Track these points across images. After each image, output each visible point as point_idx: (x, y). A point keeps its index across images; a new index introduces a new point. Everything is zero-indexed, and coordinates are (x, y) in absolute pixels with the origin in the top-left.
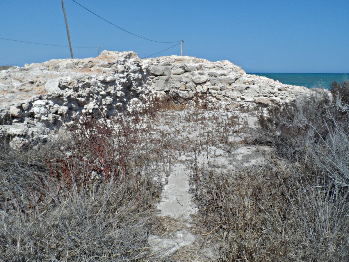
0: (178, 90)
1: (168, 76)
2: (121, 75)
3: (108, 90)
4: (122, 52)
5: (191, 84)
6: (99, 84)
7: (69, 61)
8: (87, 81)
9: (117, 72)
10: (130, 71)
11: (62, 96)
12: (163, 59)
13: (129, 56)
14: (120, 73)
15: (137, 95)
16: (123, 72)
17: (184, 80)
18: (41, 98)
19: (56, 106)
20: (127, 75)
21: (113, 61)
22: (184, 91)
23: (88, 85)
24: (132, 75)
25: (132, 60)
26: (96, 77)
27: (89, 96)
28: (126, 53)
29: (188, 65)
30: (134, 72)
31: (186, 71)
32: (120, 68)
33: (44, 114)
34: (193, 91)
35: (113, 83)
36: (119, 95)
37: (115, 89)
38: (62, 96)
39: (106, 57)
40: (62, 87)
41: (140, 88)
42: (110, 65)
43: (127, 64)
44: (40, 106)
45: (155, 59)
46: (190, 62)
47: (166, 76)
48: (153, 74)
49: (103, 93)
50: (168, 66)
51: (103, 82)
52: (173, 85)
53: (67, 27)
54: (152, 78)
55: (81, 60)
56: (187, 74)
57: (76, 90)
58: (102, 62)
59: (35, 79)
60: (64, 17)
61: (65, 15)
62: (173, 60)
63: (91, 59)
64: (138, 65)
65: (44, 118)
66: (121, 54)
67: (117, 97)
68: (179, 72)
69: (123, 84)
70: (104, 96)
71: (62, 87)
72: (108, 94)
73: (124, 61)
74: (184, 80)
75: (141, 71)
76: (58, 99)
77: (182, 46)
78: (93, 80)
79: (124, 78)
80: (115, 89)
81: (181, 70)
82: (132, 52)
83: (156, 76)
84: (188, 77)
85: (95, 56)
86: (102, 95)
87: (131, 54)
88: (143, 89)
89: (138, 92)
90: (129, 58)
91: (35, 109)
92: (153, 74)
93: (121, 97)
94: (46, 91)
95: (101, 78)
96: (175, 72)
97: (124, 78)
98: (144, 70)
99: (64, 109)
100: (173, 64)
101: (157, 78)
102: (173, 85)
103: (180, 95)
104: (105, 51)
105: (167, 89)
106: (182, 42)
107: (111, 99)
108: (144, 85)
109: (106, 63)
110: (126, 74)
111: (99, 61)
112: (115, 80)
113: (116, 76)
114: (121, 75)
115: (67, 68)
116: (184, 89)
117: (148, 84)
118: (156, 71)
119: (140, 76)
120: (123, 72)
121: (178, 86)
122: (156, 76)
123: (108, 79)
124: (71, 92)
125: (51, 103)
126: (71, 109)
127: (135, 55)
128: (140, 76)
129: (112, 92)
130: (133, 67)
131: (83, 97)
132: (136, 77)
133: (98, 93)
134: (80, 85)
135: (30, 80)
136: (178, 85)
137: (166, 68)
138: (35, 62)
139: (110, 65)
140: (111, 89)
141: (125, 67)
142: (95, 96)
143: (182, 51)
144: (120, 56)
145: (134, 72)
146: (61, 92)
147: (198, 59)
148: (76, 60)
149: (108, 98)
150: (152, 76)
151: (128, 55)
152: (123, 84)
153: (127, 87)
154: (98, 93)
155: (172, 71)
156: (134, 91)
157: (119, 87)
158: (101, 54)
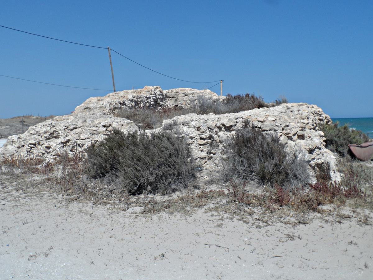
0: (182, 105)
1: (176, 98)
2: (153, 96)
3: (148, 101)
4: (154, 86)
5: (188, 102)
6: (144, 98)
7: (132, 90)
8: (140, 96)
9: (151, 94)
10: (157, 94)
11: (133, 100)
12: (175, 90)
13: (157, 88)
14: (153, 95)
15: (160, 106)
16: (154, 94)
17: (185, 99)
18: (127, 100)
19: (131, 103)
20: (156, 96)
21: (149, 90)
22: (185, 105)
23: (141, 98)
24: (158, 96)
25: (158, 90)
26: (143, 95)
27: (141, 102)
28: (155, 87)
29: (187, 92)
30: (159, 95)
31: (186, 95)
32: (153, 93)
33: (129, 104)
34: (189, 105)
35: (149, 98)
36: (152, 103)
37: (150, 100)
38: (133, 100)
39: (147, 88)
40: (133, 97)
41: (162, 103)
42: (149, 91)
43: (155, 91)
44: (127, 102)
45: (170, 90)
46: (188, 90)
47: (175, 98)
48: (169, 97)
49: (146, 101)
50: (177, 93)
51: (146, 97)
52: (180, 102)
53: (112, 74)
54: (168, 99)
55: (137, 90)
56: (186, 97)
57: (137, 98)
58: (145, 90)
59: (122, 96)
60: (110, 66)
61: (111, 64)
62: (180, 90)
63: (141, 89)
64: (161, 92)
65: (128, 105)
66: (153, 87)
67: (151, 104)
68: (182, 96)
69: (154, 99)
70: (146, 103)
71: (133, 97)
72: (148, 102)
73: (154, 90)
74: (185, 100)
75: (162, 95)
76: (132, 101)
77: (221, 86)
78: (142, 96)
79: (154, 97)
80: (150, 100)
81: (183, 95)
82: (158, 86)
83: (170, 98)
84: (186, 98)
85: (142, 88)
86: (145, 102)
87: (158, 87)
88: (164, 104)
89: (161, 104)
90: (157, 89)
91: (126, 103)
92: (169, 97)
93: (153, 105)
94: (128, 98)
95: (145, 96)
96: (181, 96)
97: (154, 97)
98: (164, 95)
99: (133, 104)
100: (179, 92)
101: (171, 98)
102: (180, 102)
103: (183, 107)
104: (146, 86)
105: (176, 104)
106: (221, 81)
107: (149, 104)
108: (164, 102)
109: (147, 91)
110: (155, 95)
111: (144, 90)
112: (150, 97)
113: (151, 96)
114: (153, 96)
115: (131, 93)
116: (185, 104)
117: (166, 102)
118: (170, 95)
119: (162, 97)
120: (154, 94)
121: (182, 103)
122: (170, 98)
123: (148, 97)
124: (136, 99)
125: (130, 102)
126: (135, 105)
127: (159, 88)
128: (162, 97)
129: (149, 102)
130: (158, 93)
131: (139, 101)
132: (160, 97)
133: (144, 101)
134: (138, 97)
135: (121, 96)
136: (182, 102)
137: (176, 94)
138: (119, 91)
139: (149, 91)
140: (149, 100)
141: (155, 92)
142: (143, 102)
143: (221, 91)
144: (153, 88)
145: (159, 95)
146: (133, 98)
147: (193, 89)
148: (135, 90)
149: (148, 104)
150: (168, 98)
151: (156, 88)
152: (154, 99)
153: (156, 101)
154: (144, 101)
155: (179, 95)
156: (159, 104)
157: (152, 100)
158: (145, 88)
